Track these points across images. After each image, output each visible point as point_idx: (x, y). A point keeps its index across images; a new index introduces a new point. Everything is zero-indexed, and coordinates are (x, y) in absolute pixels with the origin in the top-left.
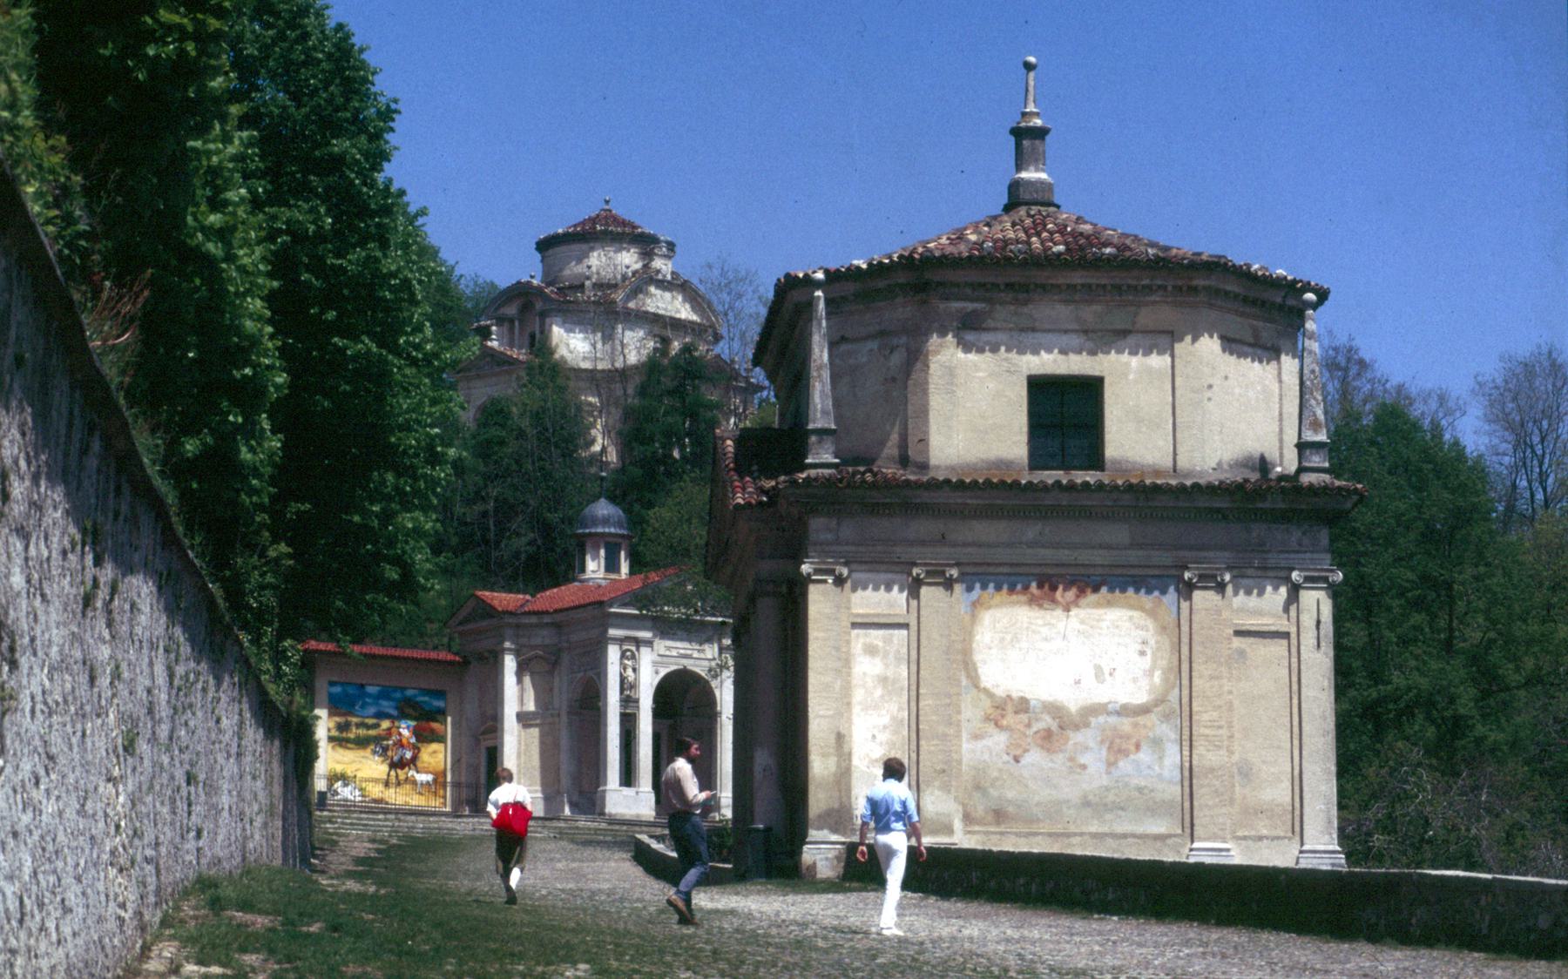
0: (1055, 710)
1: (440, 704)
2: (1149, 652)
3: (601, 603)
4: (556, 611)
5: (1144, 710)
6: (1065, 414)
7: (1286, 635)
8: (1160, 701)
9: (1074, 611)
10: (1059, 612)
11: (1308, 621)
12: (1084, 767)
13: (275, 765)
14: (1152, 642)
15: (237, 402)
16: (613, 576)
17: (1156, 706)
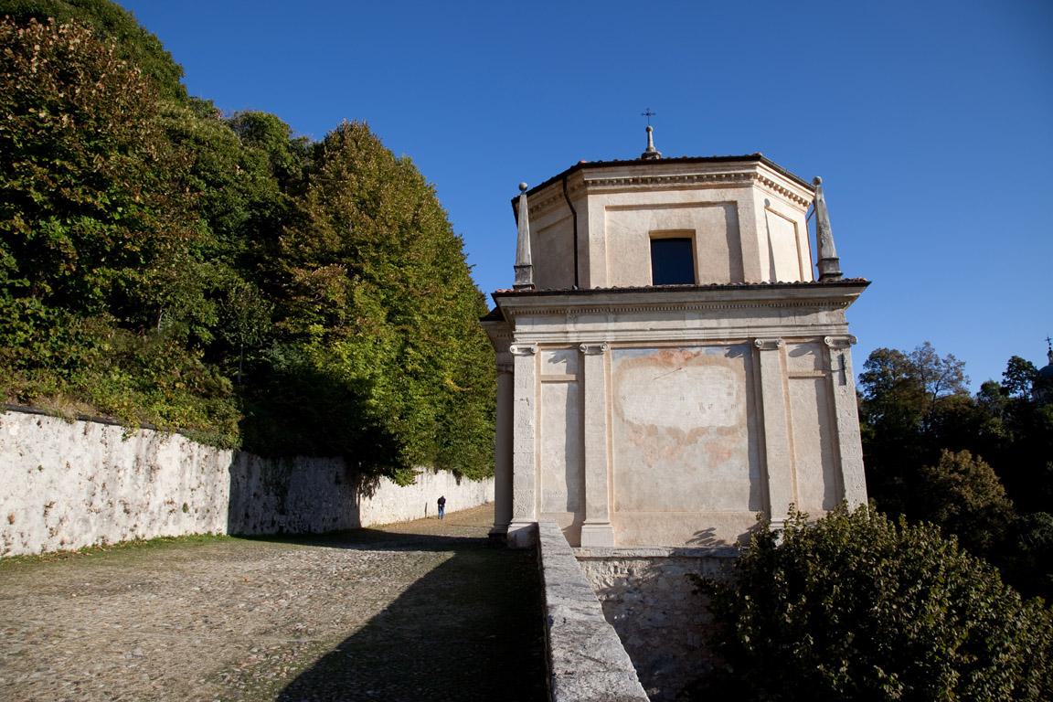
0: (674, 432)
14: (735, 386)
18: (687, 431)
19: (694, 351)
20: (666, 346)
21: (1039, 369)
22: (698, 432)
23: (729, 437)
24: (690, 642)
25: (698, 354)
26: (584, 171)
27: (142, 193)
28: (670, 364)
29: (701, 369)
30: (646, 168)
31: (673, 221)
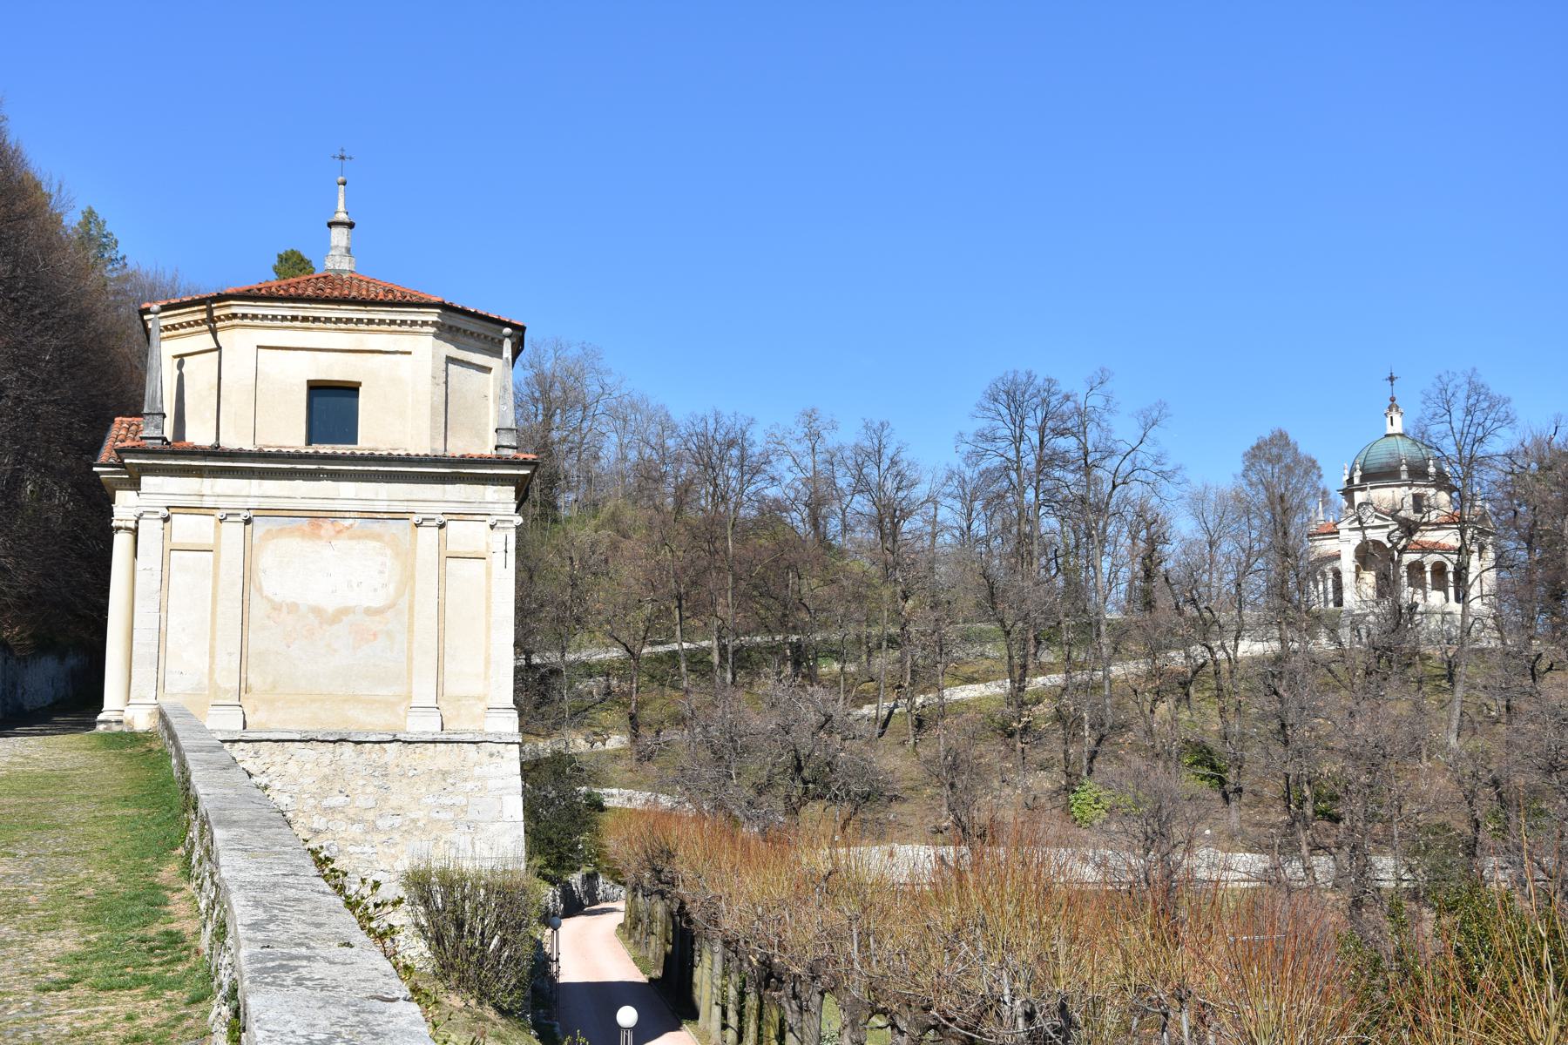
0: (317, 611)
18: (330, 610)
20: (316, 516)
21: (562, 980)
22: (343, 612)
23: (377, 618)
24: (315, 826)
27: (635, 890)
28: (320, 537)
29: (353, 543)
30: (298, 288)
31: (335, 369)
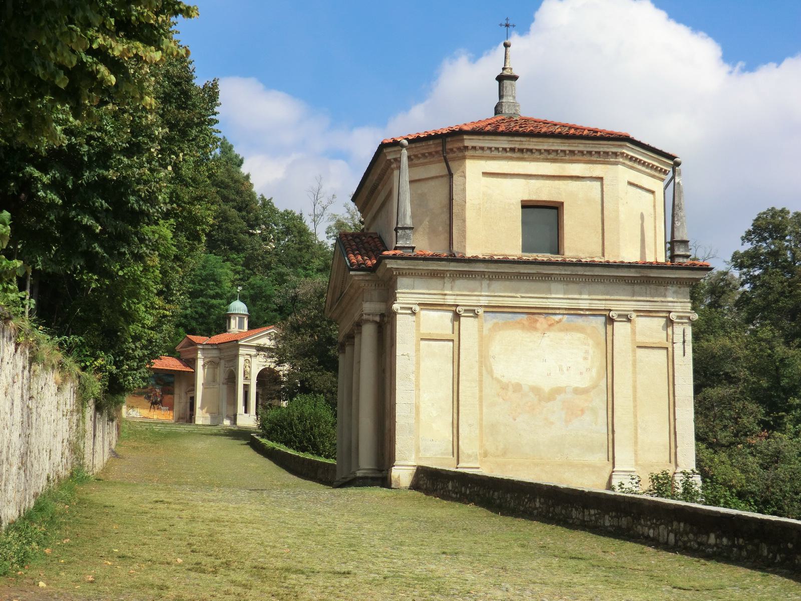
0: (536, 390)
1: (171, 379)
2: (590, 358)
3: (237, 341)
4: (219, 344)
5: (585, 391)
6: (543, 217)
7: (667, 348)
8: (594, 387)
9: (548, 334)
10: (538, 334)
11: (678, 338)
12: (552, 423)
13: (531, 140)
14: (591, 351)
15: (65, 187)
16: (241, 330)
17: (594, 388)
19: (557, 318)
22: (558, 391)
25: (560, 321)
26: (465, 137)
29: (562, 334)
